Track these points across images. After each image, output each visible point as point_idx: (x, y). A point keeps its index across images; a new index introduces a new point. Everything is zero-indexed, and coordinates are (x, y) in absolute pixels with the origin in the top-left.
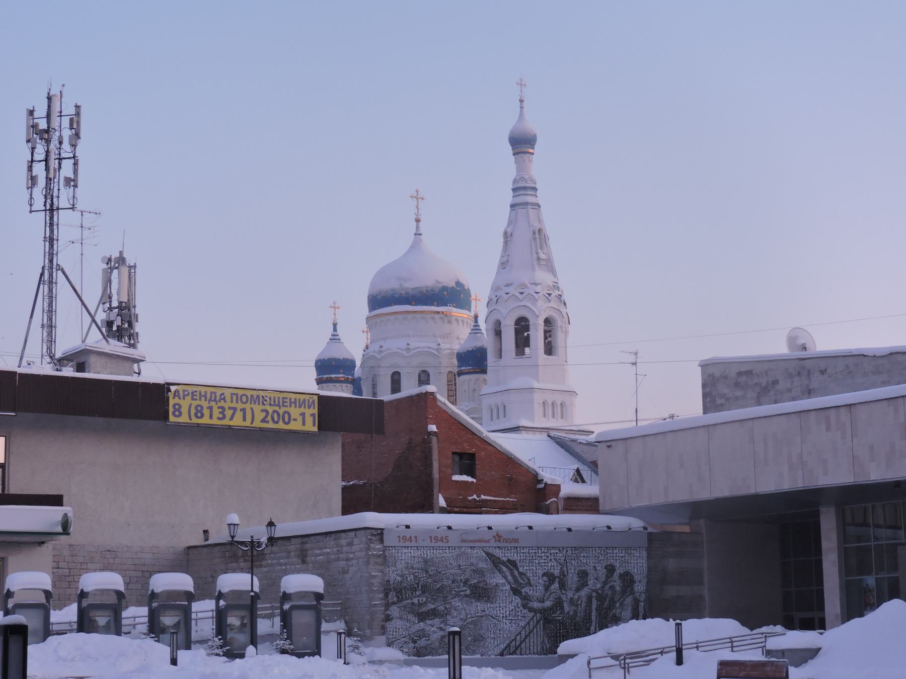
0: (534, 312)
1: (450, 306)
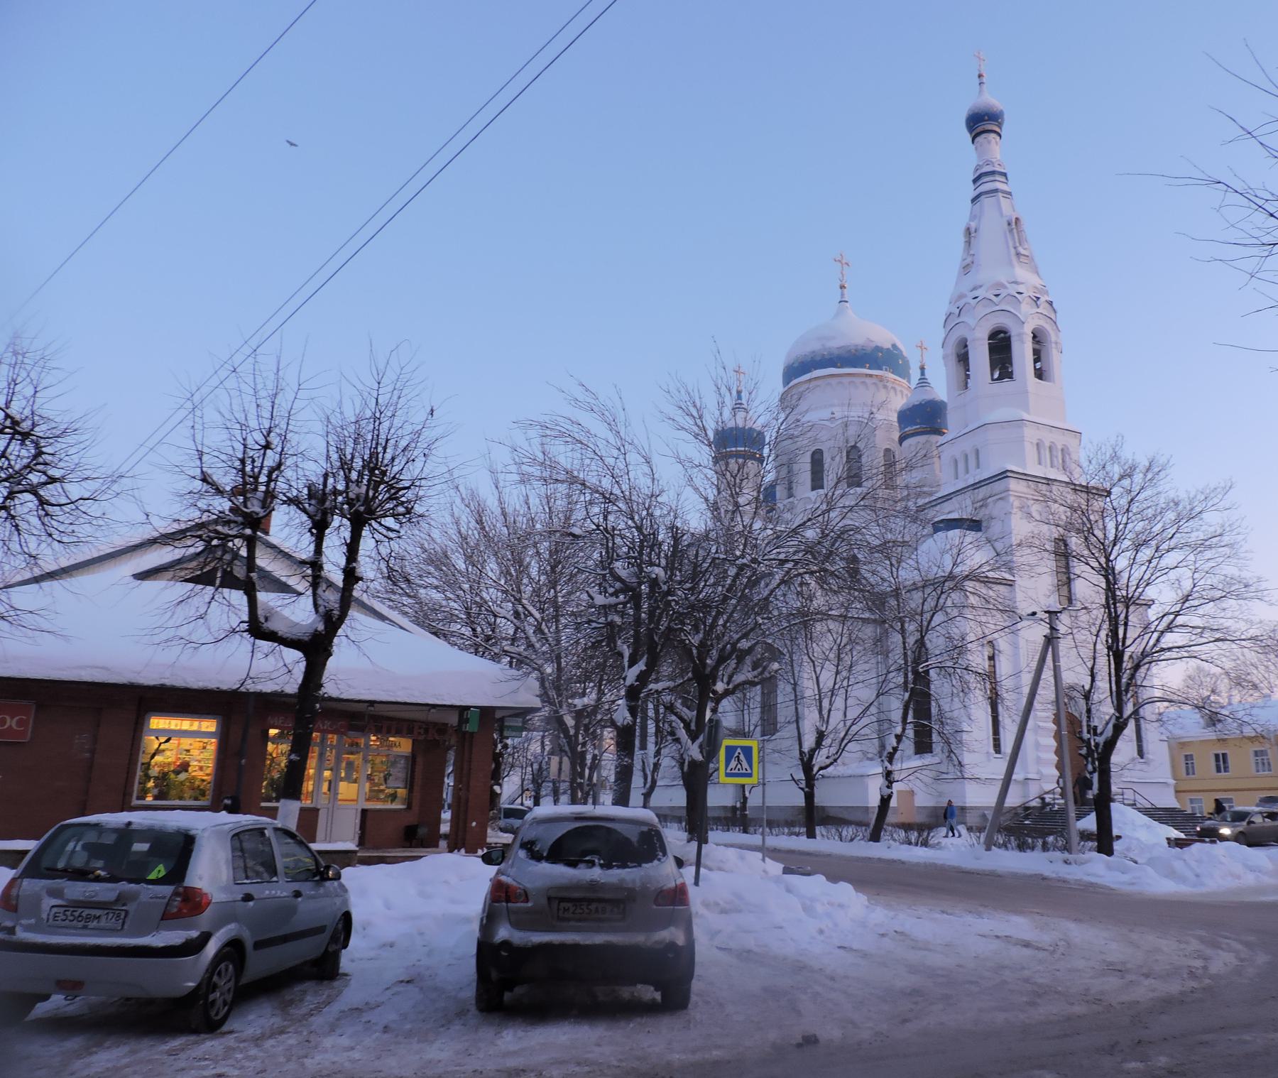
0: (1016, 315)
1: (886, 370)
